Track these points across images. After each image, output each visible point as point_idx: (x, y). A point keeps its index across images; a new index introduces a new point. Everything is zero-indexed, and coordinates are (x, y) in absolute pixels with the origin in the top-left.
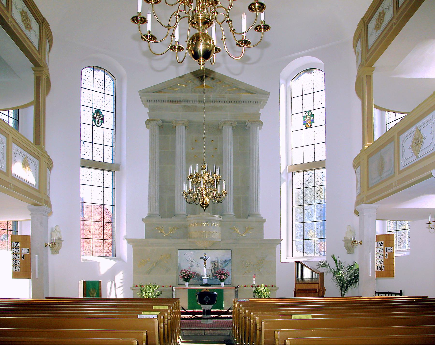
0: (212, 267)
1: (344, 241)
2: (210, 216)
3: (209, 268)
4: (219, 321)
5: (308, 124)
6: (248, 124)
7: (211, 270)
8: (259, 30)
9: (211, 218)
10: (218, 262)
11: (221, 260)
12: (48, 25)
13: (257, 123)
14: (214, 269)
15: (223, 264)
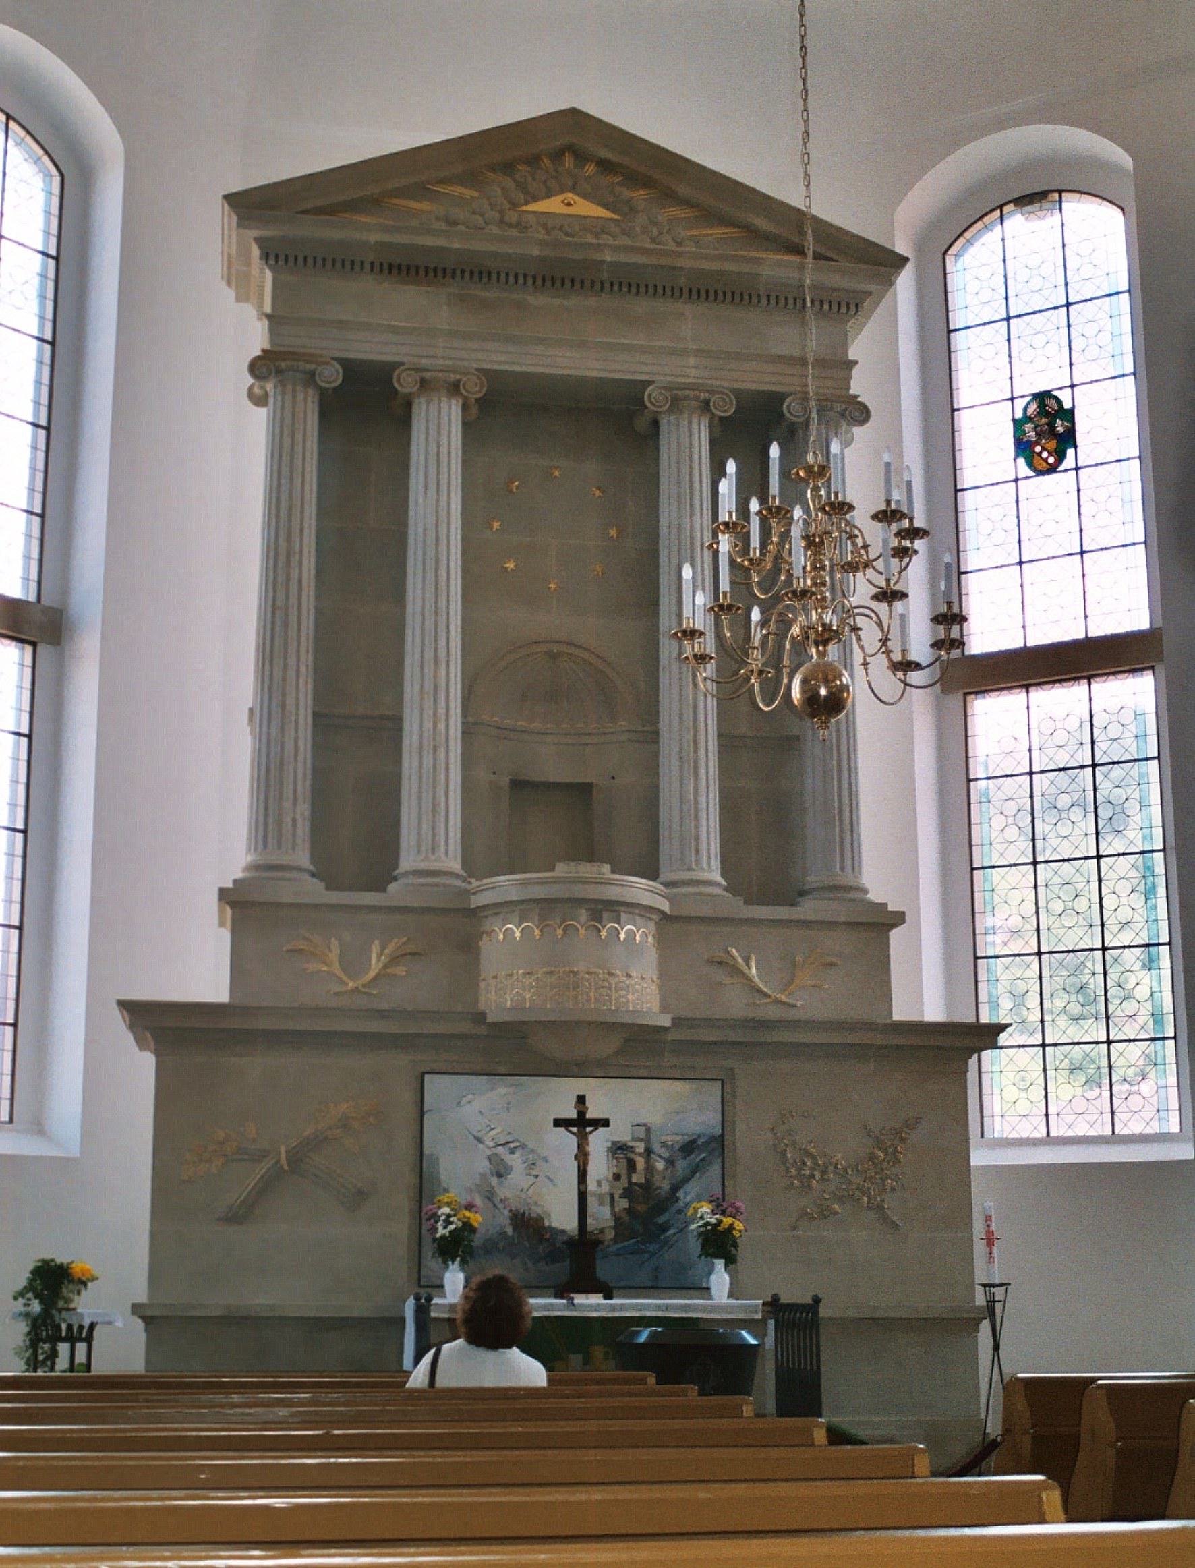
0: (617, 1177)
5: (1045, 455)
7: (612, 1196)
9: (613, 893)
10: (649, 1151)
11: (663, 1139)
14: (627, 1193)
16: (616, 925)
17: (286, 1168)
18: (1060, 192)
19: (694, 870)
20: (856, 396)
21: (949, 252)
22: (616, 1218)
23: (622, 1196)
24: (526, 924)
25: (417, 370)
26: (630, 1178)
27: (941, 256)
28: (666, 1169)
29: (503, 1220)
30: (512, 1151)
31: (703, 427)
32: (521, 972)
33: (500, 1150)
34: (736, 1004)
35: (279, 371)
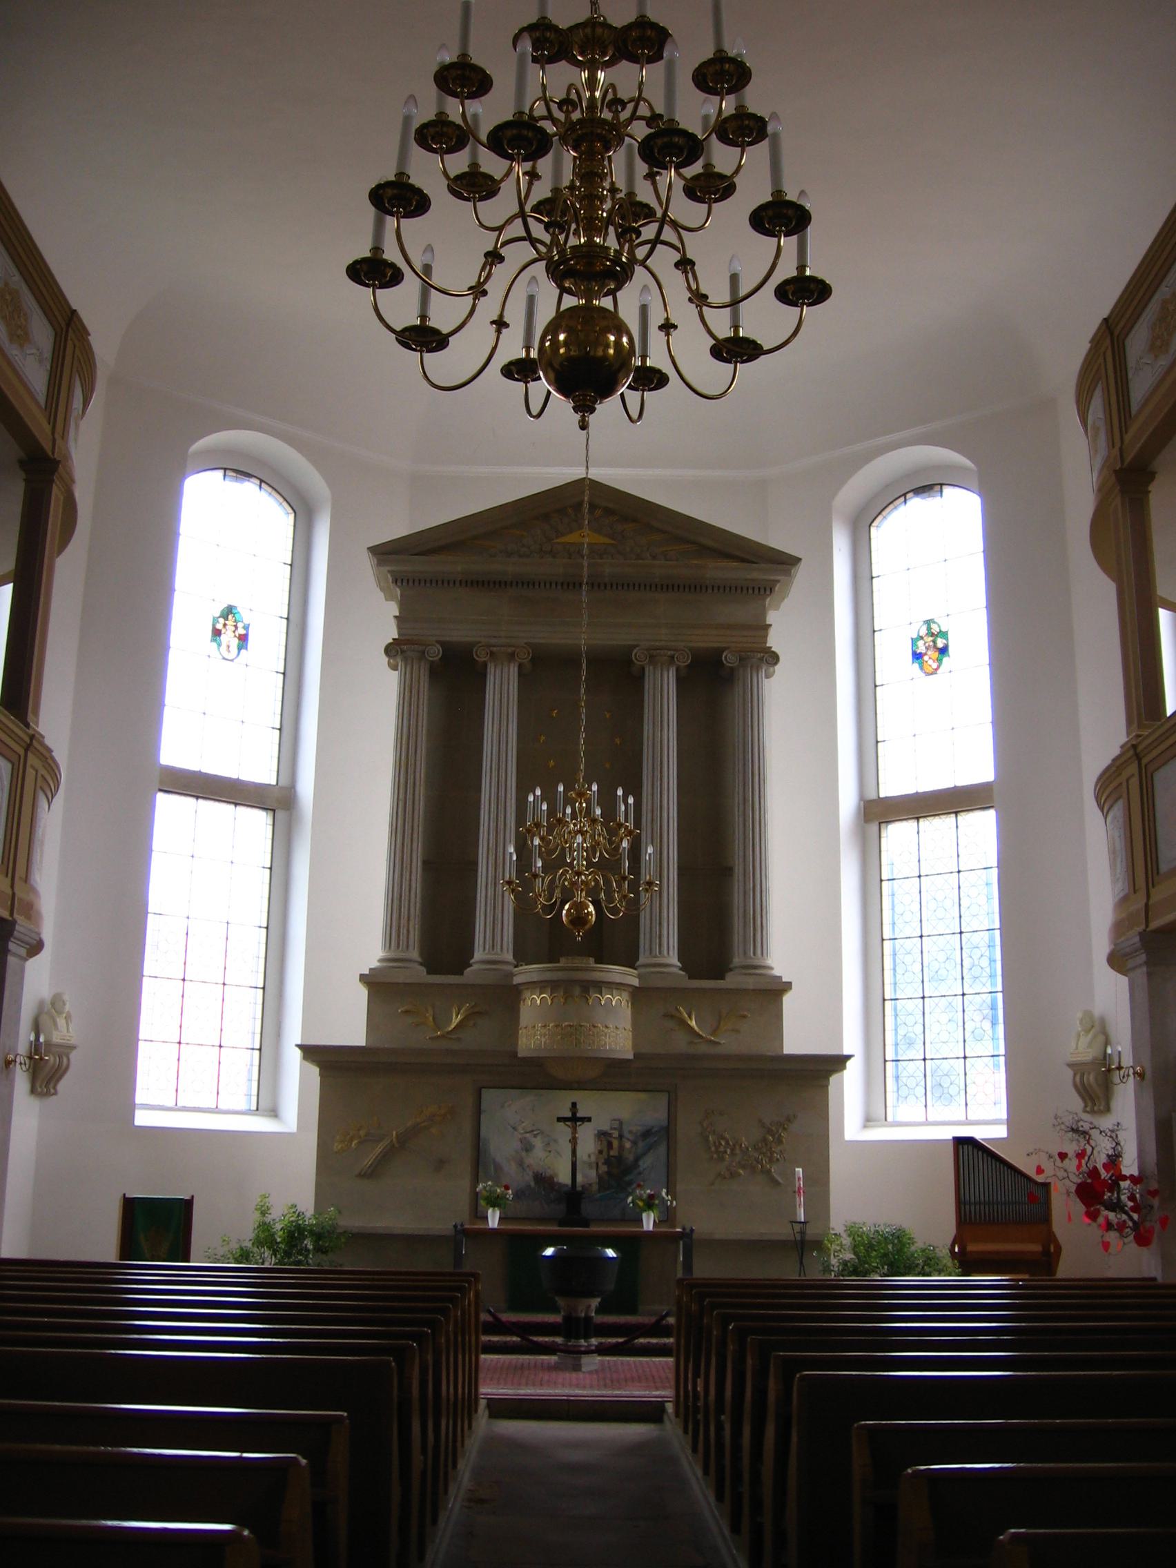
0: (601, 1152)
1: (1070, 1065)
2: (594, 970)
3: (589, 1156)
4: (622, 1363)
6: (729, 659)
7: (597, 1164)
8: (791, 297)
10: (621, 1136)
12: (83, 333)
13: (759, 655)
14: (607, 1162)
15: (641, 1144)
16: (599, 996)
17: (397, 1145)
18: (941, 485)
19: (659, 957)
20: (771, 647)
21: (873, 524)
22: (600, 1177)
23: (604, 1164)
24: (544, 995)
25: (489, 646)
26: (609, 1152)
27: (868, 528)
28: (632, 1147)
29: (529, 1178)
30: (535, 1136)
31: (671, 675)
32: (540, 1025)
33: (528, 1135)
34: (680, 1043)
35: (403, 652)
